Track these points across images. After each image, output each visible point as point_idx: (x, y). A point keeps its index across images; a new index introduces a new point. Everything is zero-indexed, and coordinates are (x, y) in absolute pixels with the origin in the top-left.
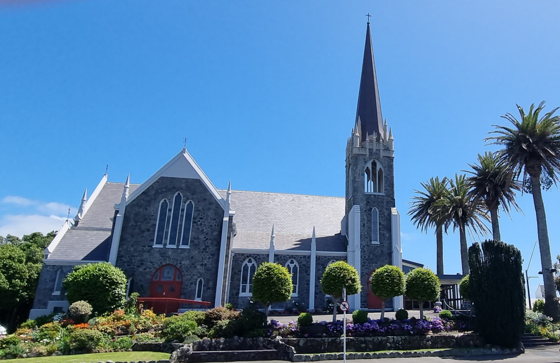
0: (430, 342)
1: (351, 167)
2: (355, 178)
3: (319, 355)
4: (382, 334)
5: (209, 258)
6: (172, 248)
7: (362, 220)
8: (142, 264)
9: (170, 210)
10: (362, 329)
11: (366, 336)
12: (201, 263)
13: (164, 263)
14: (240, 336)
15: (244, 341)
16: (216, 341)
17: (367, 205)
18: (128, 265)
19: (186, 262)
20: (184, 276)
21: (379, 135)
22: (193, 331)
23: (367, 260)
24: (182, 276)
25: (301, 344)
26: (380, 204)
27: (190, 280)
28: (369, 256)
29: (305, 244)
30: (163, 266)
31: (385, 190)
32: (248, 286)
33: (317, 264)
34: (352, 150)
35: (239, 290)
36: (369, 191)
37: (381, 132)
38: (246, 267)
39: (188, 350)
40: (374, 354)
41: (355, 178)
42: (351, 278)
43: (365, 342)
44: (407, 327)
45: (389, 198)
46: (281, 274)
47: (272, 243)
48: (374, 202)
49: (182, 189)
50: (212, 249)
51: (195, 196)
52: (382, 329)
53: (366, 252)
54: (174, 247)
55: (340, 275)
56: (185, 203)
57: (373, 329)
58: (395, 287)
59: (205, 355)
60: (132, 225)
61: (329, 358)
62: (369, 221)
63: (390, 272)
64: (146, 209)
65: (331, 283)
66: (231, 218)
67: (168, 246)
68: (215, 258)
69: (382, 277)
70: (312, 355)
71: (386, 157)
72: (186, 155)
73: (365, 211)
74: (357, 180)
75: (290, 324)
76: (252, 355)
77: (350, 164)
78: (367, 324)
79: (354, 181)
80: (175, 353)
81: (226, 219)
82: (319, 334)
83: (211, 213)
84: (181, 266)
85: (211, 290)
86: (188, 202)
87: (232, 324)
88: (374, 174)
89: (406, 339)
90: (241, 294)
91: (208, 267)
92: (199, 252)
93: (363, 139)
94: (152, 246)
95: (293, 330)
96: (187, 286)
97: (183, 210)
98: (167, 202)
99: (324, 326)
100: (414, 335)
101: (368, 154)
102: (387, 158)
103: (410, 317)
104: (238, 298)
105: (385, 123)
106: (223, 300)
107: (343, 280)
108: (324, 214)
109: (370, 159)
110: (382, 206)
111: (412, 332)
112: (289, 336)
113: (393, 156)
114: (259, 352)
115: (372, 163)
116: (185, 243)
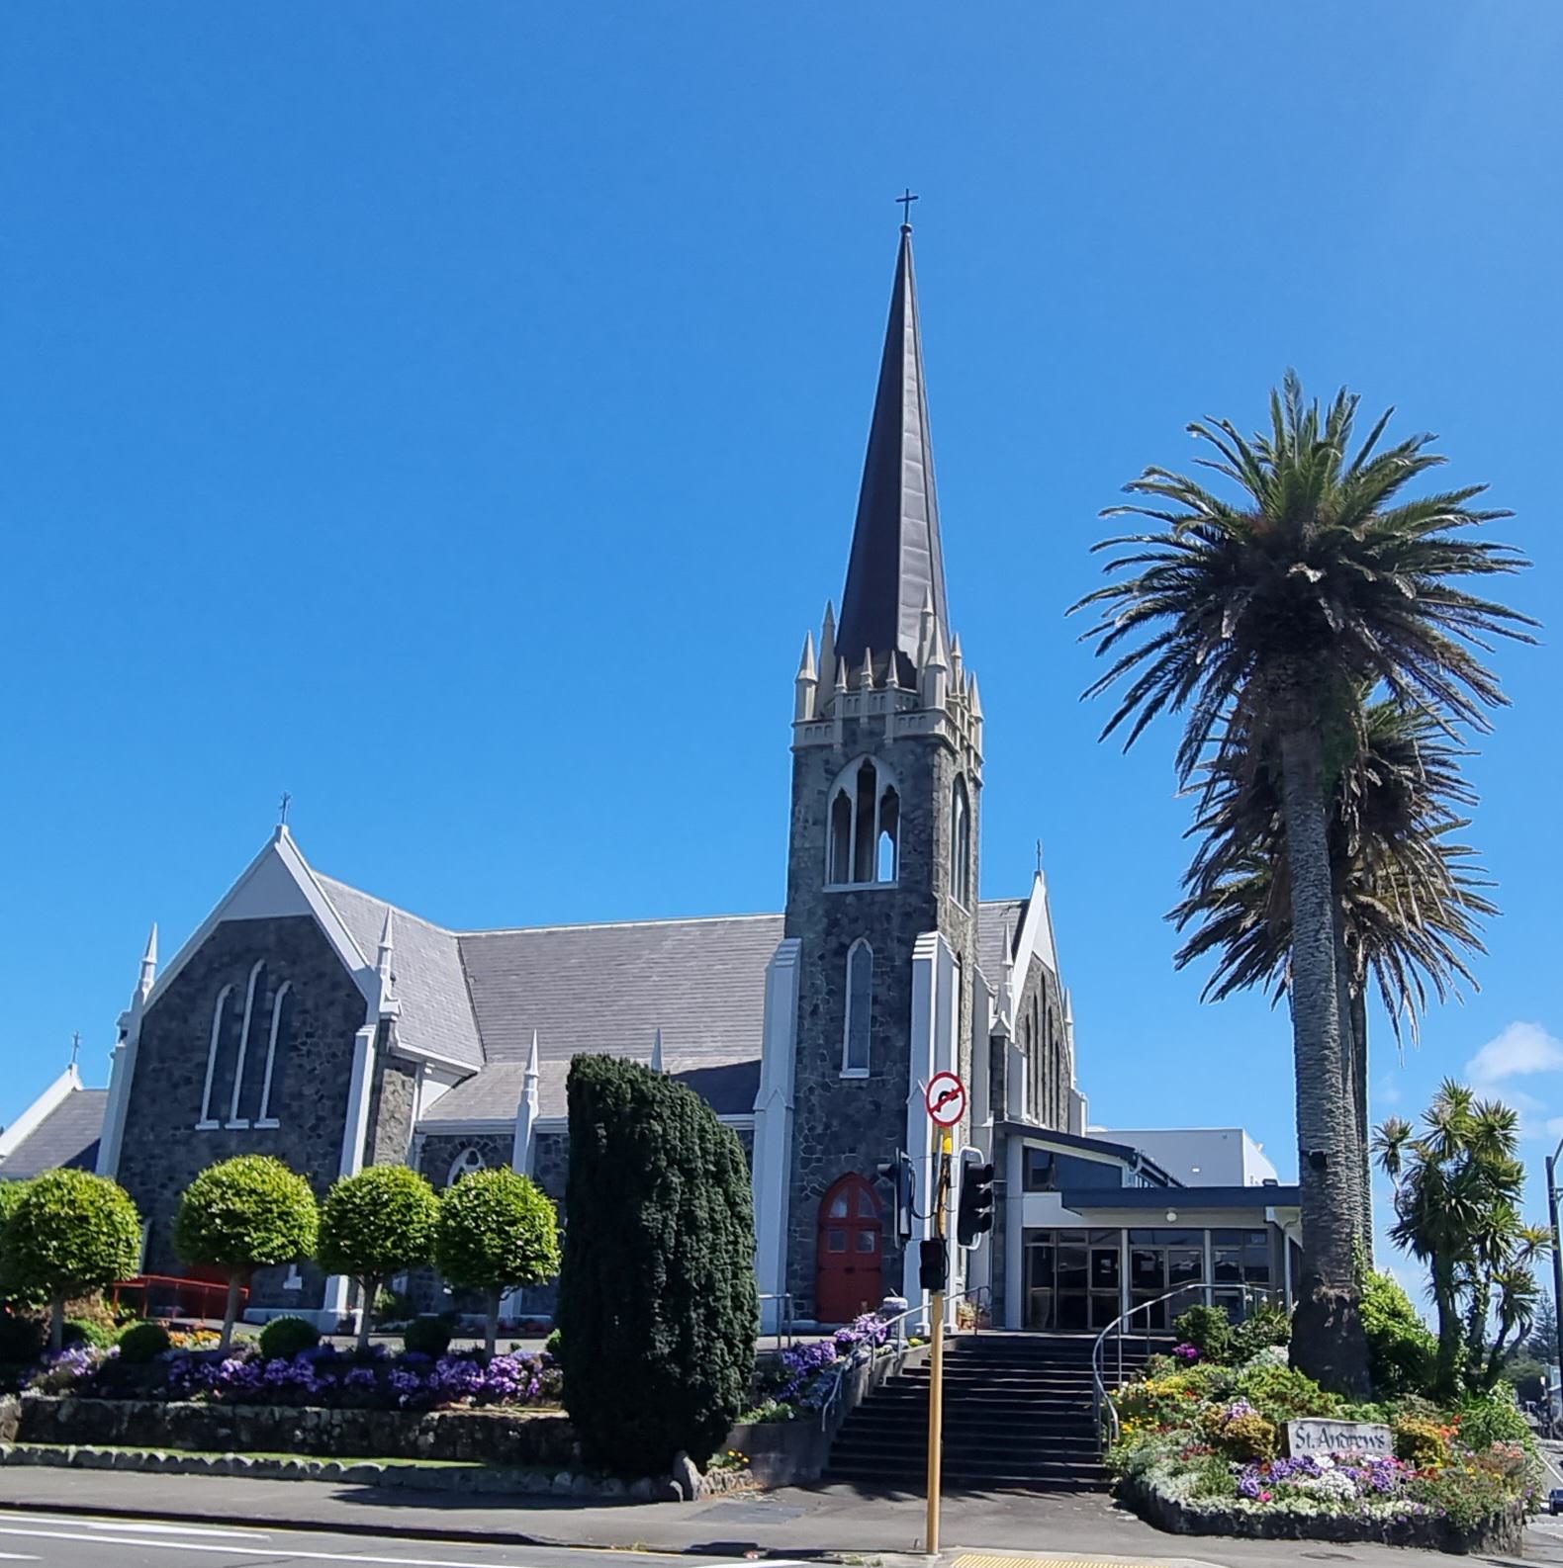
0: (431, 1437)
8: (171, 1179)
17: (828, 933)
18: (142, 1184)
23: (819, 1139)
26: (877, 926)
28: (827, 1126)
45: (914, 900)
48: (855, 920)
53: (818, 1112)
60: (154, 1070)
64: (186, 1021)
66: (385, 1026)
71: (906, 738)
73: (821, 957)
86: (283, 989)
89: (353, 1422)
94: (192, 1127)
102: (911, 744)
109: (849, 760)
110: (886, 934)
115: (860, 774)
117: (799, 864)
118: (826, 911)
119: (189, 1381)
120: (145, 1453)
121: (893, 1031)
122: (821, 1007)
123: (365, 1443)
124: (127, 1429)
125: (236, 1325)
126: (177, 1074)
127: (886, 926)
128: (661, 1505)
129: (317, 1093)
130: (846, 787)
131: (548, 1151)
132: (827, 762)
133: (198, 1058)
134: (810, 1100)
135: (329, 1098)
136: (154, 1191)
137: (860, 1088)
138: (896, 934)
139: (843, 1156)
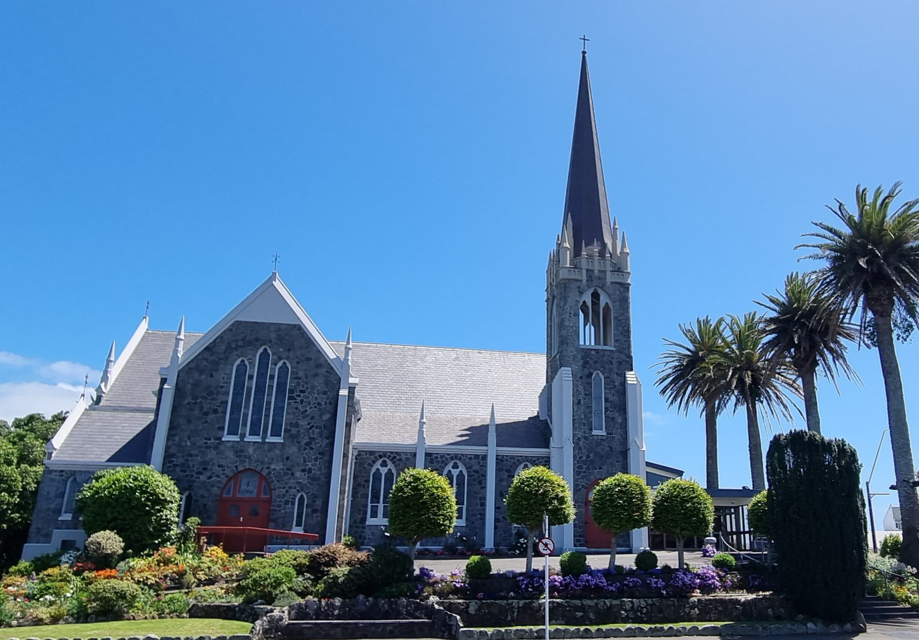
1: (556, 301)
2: (562, 320)
4: (611, 595)
5: (316, 459)
6: (255, 442)
7: (576, 393)
8: (205, 469)
9: (251, 377)
10: (577, 585)
13: (241, 468)
15: (375, 604)
16: (327, 604)
19: (277, 466)
21: (604, 245)
22: (289, 586)
23: (585, 462)
24: (271, 490)
25: (472, 609)
26: (606, 366)
27: (284, 496)
28: (588, 457)
29: (477, 434)
31: (616, 341)
32: (381, 506)
33: (498, 470)
34: (557, 272)
35: (366, 513)
36: (587, 343)
37: (608, 240)
38: (377, 474)
39: (281, 619)
40: (598, 630)
41: (562, 320)
42: (557, 495)
43: (582, 608)
44: (656, 583)
46: (437, 488)
47: (421, 432)
48: (596, 362)
49: (271, 341)
51: (291, 354)
52: (611, 585)
54: (258, 439)
55: (538, 491)
56: (276, 364)
57: (596, 585)
60: (189, 403)
62: (588, 395)
63: (625, 486)
64: (212, 376)
65: (523, 505)
66: (352, 390)
67: (249, 438)
72: (277, 284)
73: (581, 378)
74: (567, 323)
75: (453, 575)
77: (554, 297)
78: (585, 577)
79: (561, 325)
81: (344, 392)
83: (319, 383)
84: (270, 473)
85: (319, 514)
86: (280, 364)
87: (355, 575)
89: (653, 604)
90: (370, 521)
91: (315, 474)
92: (299, 449)
93: (577, 252)
96: (279, 506)
97: (272, 377)
98: (247, 363)
99: (510, 579)
100: (669, 596)
101: (585, 278)
103: (660, 565)
104: (364, 528)
105: (615, 224)
106: (339, 530)
107: (543, 500)
108: (511, 383)
109: (589, 288)
110: (611, 370)
111: (664, 592)
112: (451, 596)
113: (629, 281)
120: (582, 628)
126: (206, 407)
130: (587, 300)
132: (579, 287)
133: (221, 398)
135: (317, 427)
136: (192, 476)
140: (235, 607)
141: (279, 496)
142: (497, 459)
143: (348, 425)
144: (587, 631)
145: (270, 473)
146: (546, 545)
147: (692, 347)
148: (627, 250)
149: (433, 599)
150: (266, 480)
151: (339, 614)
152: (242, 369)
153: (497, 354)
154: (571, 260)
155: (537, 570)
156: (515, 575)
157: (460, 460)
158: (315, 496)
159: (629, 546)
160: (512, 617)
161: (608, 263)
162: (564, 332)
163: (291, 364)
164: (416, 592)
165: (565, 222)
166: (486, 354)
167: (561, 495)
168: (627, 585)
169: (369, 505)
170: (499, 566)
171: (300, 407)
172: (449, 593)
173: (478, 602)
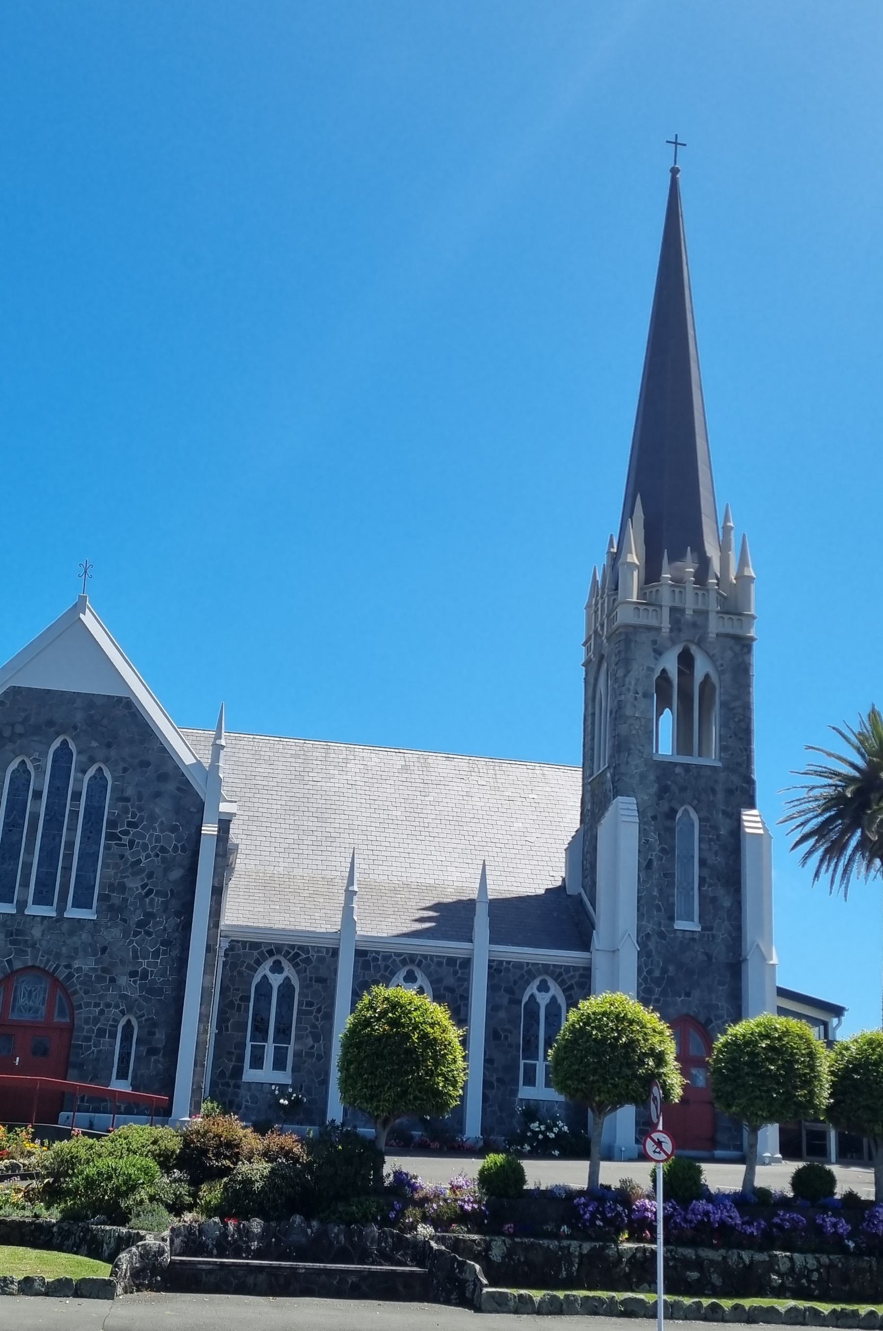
1: (604, 666)
2: (620, 706)
3: (561, 1294)
4: (749, 1243)
5: (156, 954)
6: (44, 918)
7: (644, 847)
9: (38, 795)
10: (685, 1220)
11: (717, 1247)
12: (130, 968)
13: (18, 965)
14: (308, 1217)
15: (323, 1234)
16: (238, 1229)
19: (85, 964)
20: (80, 1007)
21: (704, 563)
22: (152, 1191)
23: (658, 982)
24: (72, 1008)
25: (497, 1253)
27: (96, 1020)
28: (664, 971)
29: (453, 917)
30: (14, 972)
31: (723, 749)
33: (492, 988)
34: (612, 610)
35: (241, 1059)
37: (712, 551)
38: (264, 987)
39: (161, 1252)
40: (736, 1307)
41: (620, 706)
42: (652, 1049)
43: (698, 1264)
44: (835, 1225)
46: (432, 1025)
47: (348, 911)
48: (683, 789)
49: (75, 728)
50: (167, 923)
51: (113, 753)
52: (749, 1223)
54: (49, 911)
55: (617, 1039)
56: (84, 772)
57: (722, 1223)
58: (795, 1088)
59: (210, 1272)
61: (593, 1309)
62: (668, 851)
63: (780, 1039)
65: (588, 1065)
66: (224, 825)
67: (33, 910)
68: (175, 953)
69: (753, 1054)
70: (537, 1295)
71: (727, 635)
72: (88, 619)
73: (654, 818)
74: (629, 711)
75: (454, 1188)
76: (351, 1279)
77: (602, 658)
78: (702, 1205)
79: (618, 715)
80: (124, 1256)
81: (210, 829)
82: (549, 1228)
83: (162, 809)
84: (70, 976)
85: (160, 1057)
86: (91, 772)
87: (283, 1177)
88: (681, 694)
89: (832, 1266)
90: (250, 1075)
91: (153, 982)
92: (126, 935)
93: (651, 574)
95: (468, 1207)
96: (88, 1039)
97: (77, 796)
98: (30, 767)
99: (560, 1201)
100: (859, 1253)
101: (666, 625)
103: (840, 1191)
104: (237, 1086)
105: (727, 519)
106: (196, 1090)
107: (627, 1056)
108: (509, 821)
109: (674, 642)
111: (851, 1245)
112: (454, 1226)
113: (752, 633)
114: (372, 1273)
116: (82, 902)
117: (631, 731)
118: (658, 778)
119: (601, 1220)
120: (706, 1302)
121: (721, 892)
122: (655, 863)
123: (847, 1288)
124: (578, 1270)
125: (603, 1164)
127: (711, 798)
128: (797, 1327)
129: (144, 886)
131: (366, 966)
132: (654, 642)
134: (647, 946)
135: (158, 893)
137: (693, 939)
138: (722, 807)
139: (679, 1000)
140: (50, 1226)
141: (87, 1021)
142: (490, 967)
143: (218, 892)
144: (715, 1307)
145: (70, 976)
146: (659, 1144)
147: (860, 762)
148: (750, 572)
149: (425, 1231)
150: (65, 990)
151: (258, 1249)
152: (21, 779)
153: (481, 763)
154: (640, 589)
155: (608, 1188)
156: (571, 1195)
157: (419, 965)
158: (154, 1024)
159: (740, 1148)
160: (569, 1273)
161: (713, 596)
162: (623, 729)
163: (112, 772)
164: (392, 1215)
165: (628, 513)
166: (462, 763)
167: (659, 1049)
168: (780, 1227)
169: (522, 1062)
170: (543, 1174)
171: (128, 853)
172: (451, 1221)
173: (508, 1241)
